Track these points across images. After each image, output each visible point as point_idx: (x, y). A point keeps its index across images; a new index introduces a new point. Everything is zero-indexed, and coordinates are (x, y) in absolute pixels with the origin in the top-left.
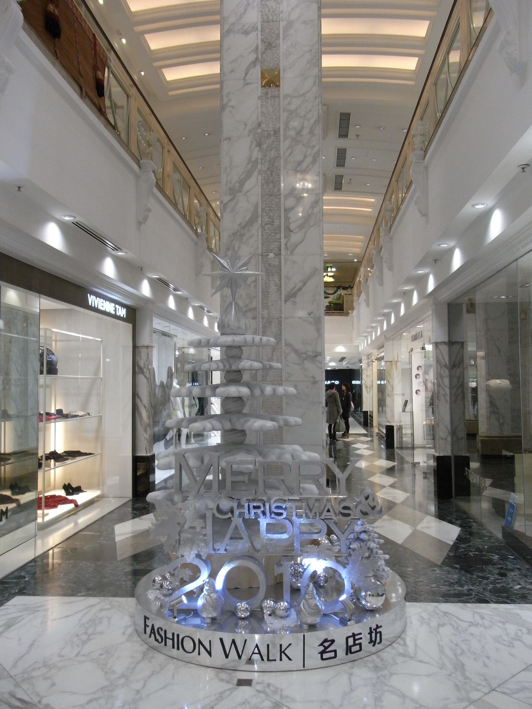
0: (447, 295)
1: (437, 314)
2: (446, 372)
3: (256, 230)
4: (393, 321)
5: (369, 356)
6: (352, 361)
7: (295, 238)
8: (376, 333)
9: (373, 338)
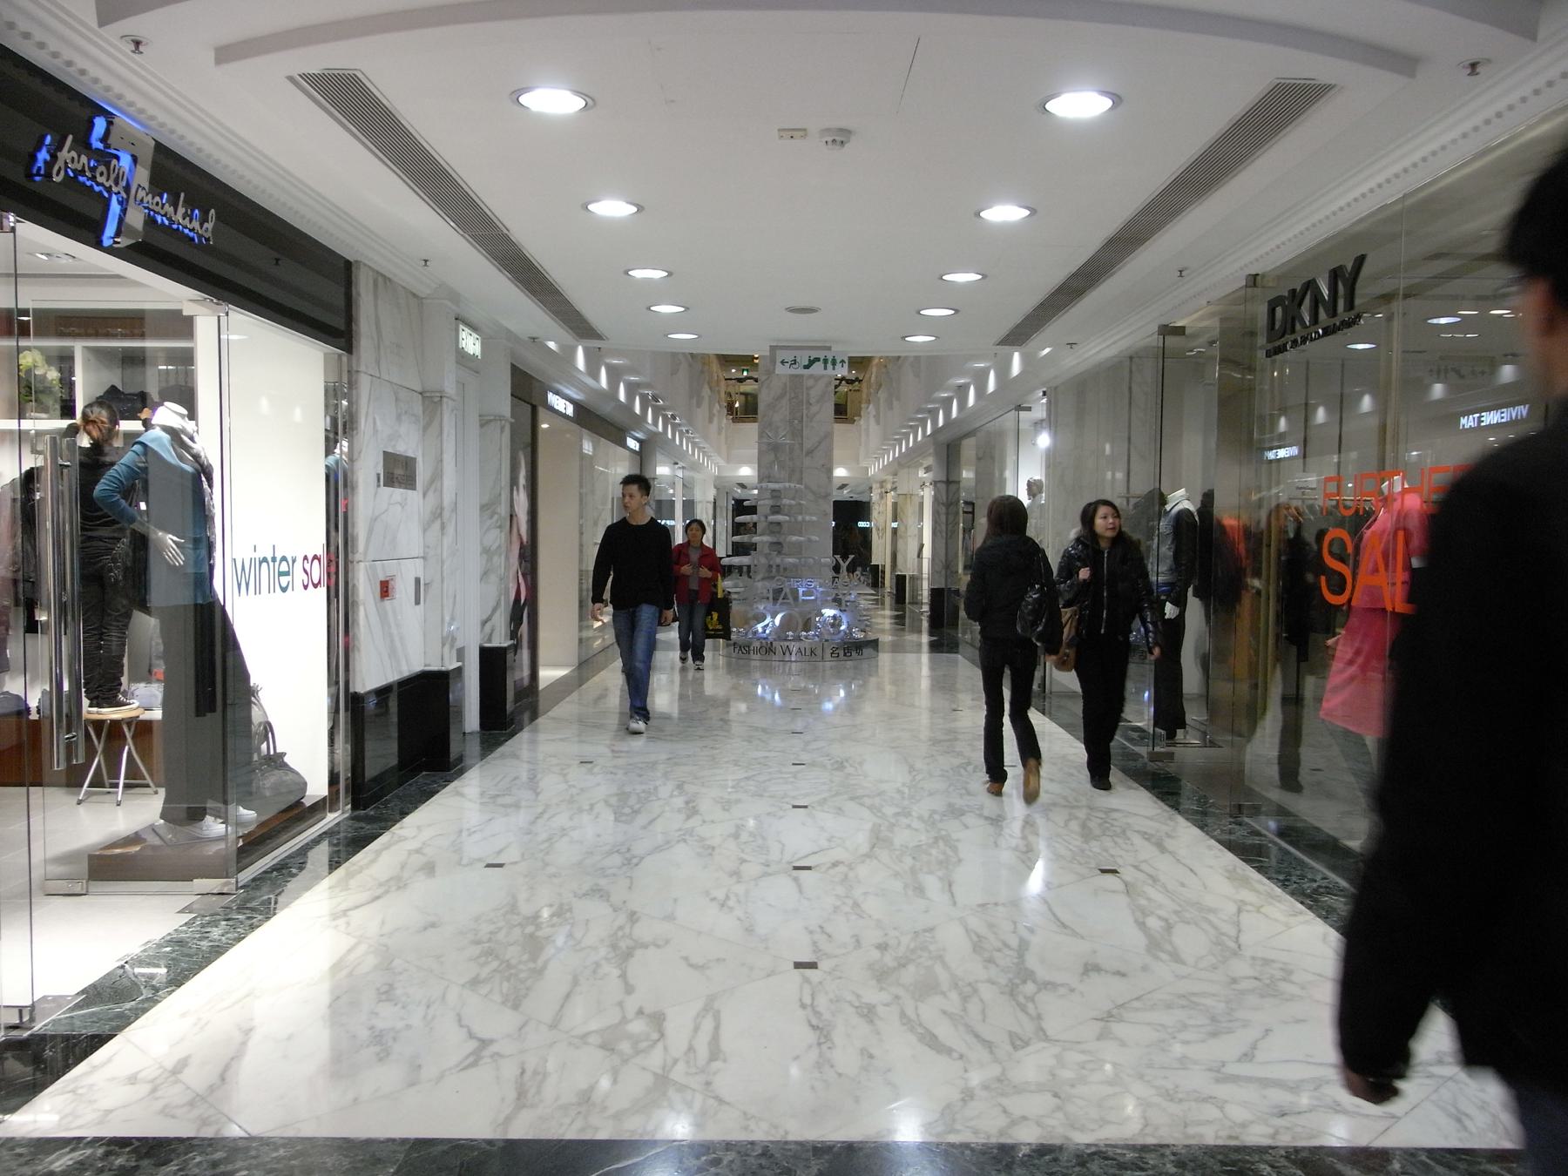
0: (942, 438)
1: (937, 454)
2: (943, 510)
3: (785, 401)
4: (991, 385)
5: (882, 483)
6: (860, 489)
7: (814, 409)
8: (935, 422)
9: (941, 423)
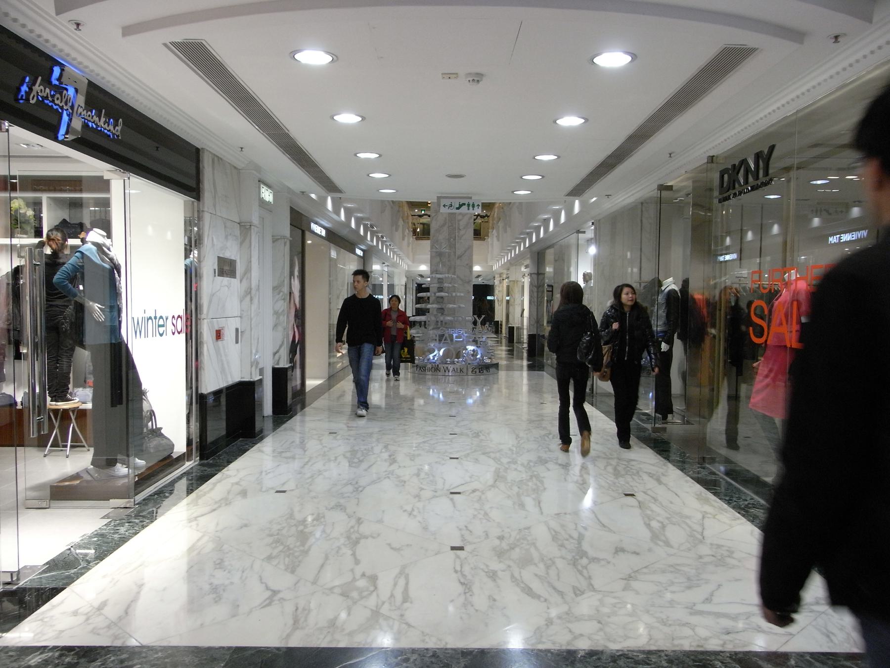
0: (535, 249)
1: (532, 258)
2: (535, 289)
3: (445, 228)
4: (563, 219)
5: (501, 275)
6: (488, 278)
7: (462, 232)
8: (531, 240)
9: (534, 240)
